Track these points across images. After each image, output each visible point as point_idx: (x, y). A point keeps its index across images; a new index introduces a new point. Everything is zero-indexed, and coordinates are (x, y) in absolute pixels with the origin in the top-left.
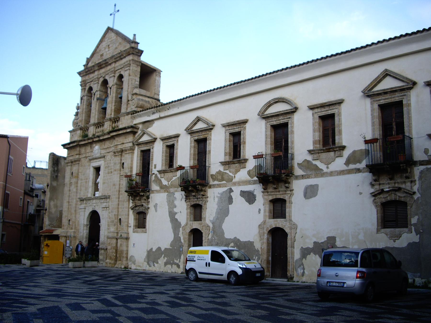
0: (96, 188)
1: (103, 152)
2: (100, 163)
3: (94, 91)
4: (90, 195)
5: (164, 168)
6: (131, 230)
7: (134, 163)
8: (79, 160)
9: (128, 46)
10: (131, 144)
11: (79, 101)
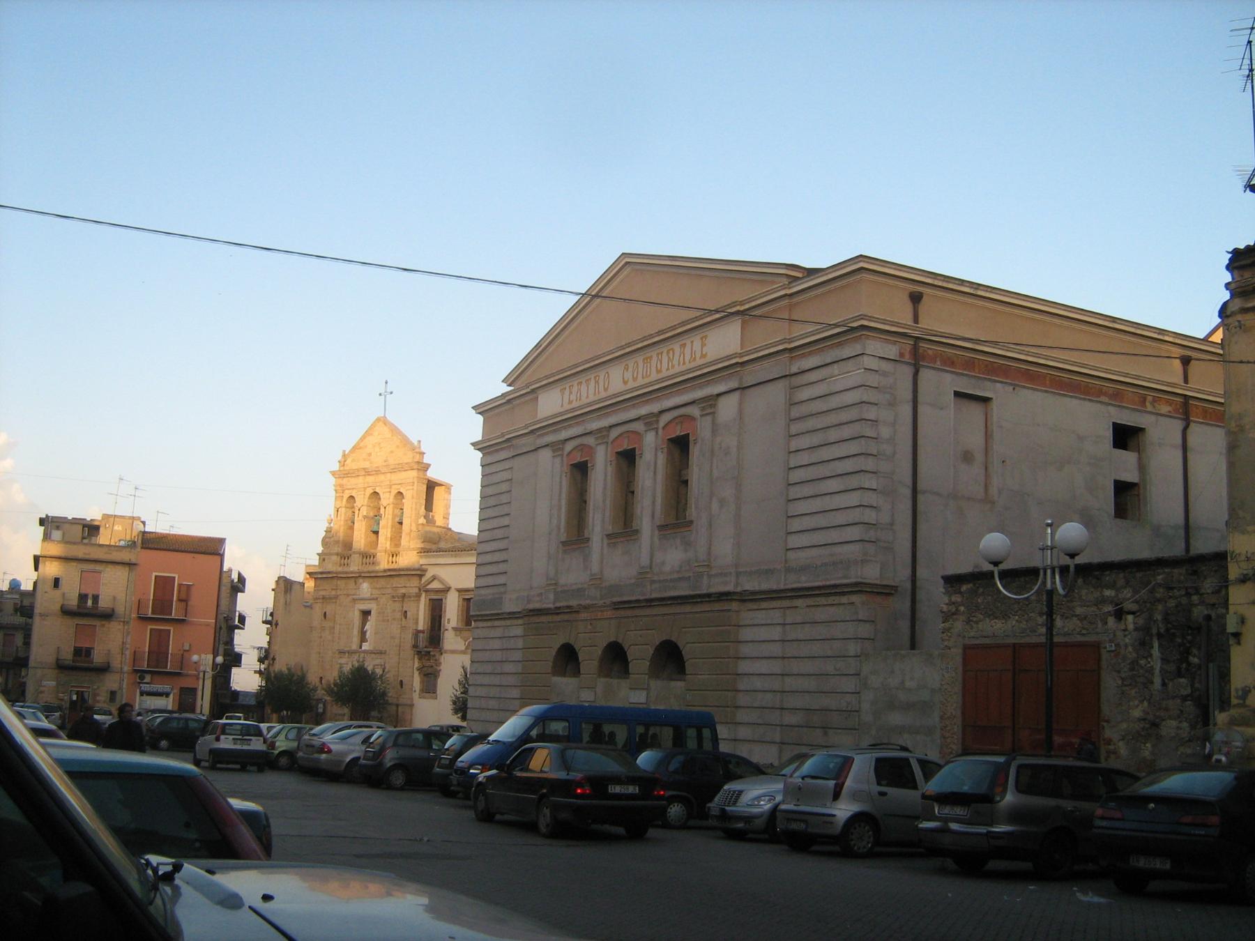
0: (363, 638)
1: (375, 592)
2: (371, 606)
3: (358, 504)
4: (354, 647)
5: (460, 626)
6: (416, 696)
7: (421, 617)
8: (336, 597)
9: (408, 458)
10: (416, 590)
11: (332, 511)
